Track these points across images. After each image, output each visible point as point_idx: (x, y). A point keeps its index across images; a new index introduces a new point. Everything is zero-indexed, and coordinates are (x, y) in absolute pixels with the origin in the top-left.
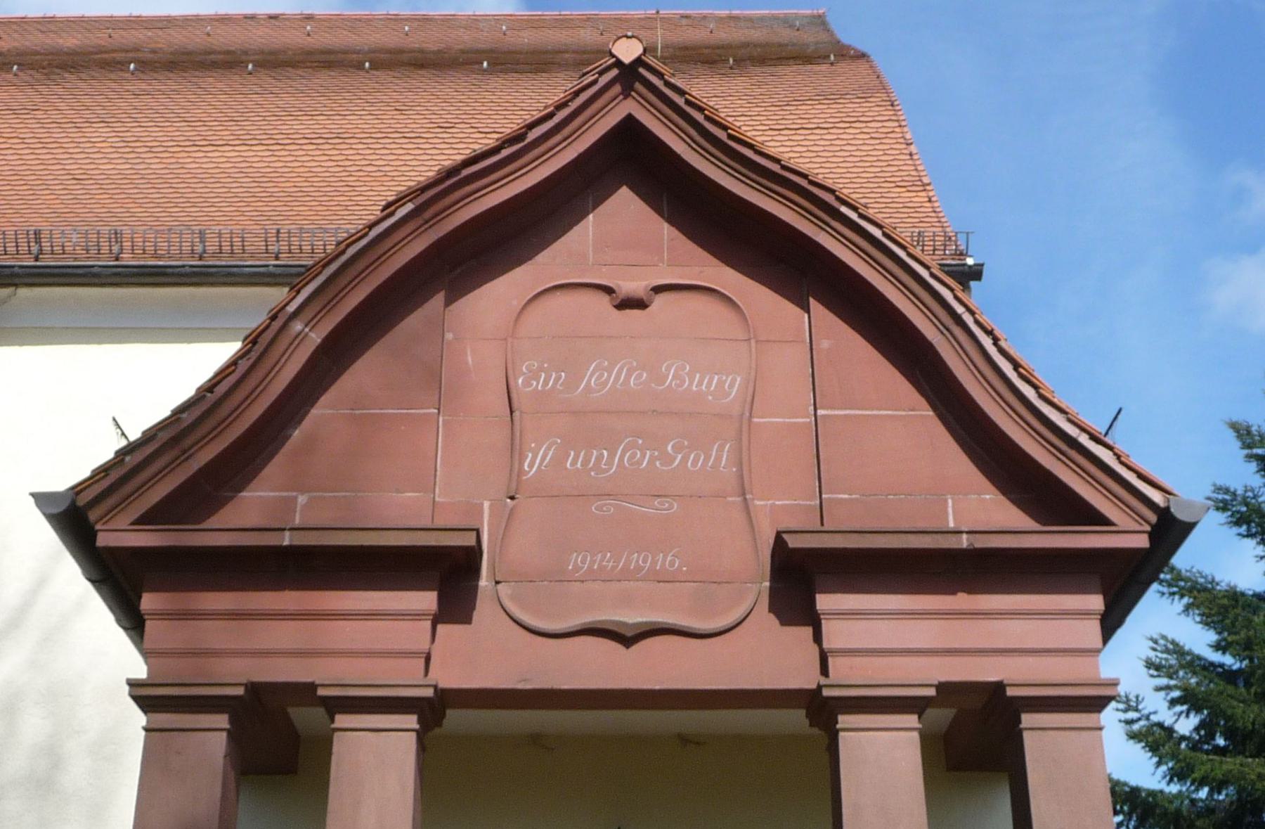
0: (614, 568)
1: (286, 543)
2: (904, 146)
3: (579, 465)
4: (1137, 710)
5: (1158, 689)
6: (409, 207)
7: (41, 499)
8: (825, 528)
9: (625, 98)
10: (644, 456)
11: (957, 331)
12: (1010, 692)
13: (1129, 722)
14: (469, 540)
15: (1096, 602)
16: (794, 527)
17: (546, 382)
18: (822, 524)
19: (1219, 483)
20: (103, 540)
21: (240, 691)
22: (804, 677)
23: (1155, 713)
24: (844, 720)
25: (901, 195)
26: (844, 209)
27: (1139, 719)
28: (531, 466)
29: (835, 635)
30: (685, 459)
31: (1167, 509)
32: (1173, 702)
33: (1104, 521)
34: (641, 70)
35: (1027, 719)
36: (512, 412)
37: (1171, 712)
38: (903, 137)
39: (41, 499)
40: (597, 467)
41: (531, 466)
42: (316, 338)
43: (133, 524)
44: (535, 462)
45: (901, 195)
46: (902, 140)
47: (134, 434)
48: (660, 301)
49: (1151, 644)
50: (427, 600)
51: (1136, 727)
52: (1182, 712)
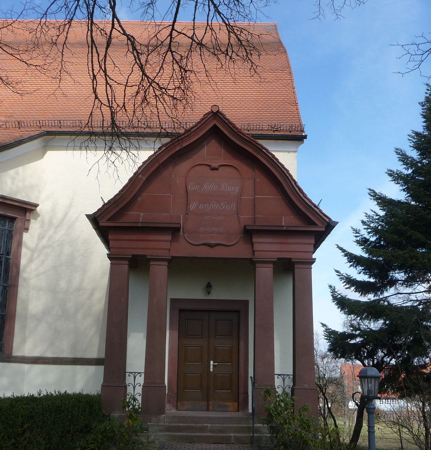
0: (209, 231)
1: (140, 226)
2: (292, 89)
3: (202, 208)
4: (359, 233)
5: (365, 229)
6: (165, 148)
7: (88, 216)
8: (256, 224)
9: (214, 120)
10: (216, 205)
11: (287, 180)
12: (293, 260)
13: (356, 237)
14: (179, 226)
15: (313, 241)
16: (248, 224)
17: (195, 188)
18: (255, 224)
19: (389, 168)
20: (101, 224)
21: (131, 257)
22: (248, 256)
23: (364, 235)
24: (257, 265)
25: (290, 107)
26: (263, 150)
27: (359, 236)
28: (191, 208)
29: (257, 247)
30: (225, 207)
31: (329, 223)
32: (369, 233)
33: (316, 225)
34: (218, 114)
35: (296, 266)
36: (187, 195)
37: (368, 236)
38: (292, 86)
39: (88, 216)
40: (206, 208)
41: (191, 208)
42: (144, 178)
43: (107, 221)
44: (193, 206)
45: (290, 107)
46: (292, 87)
47: (106, 202)
48: (221, 169)
49: (365, 215)
50: (169, 237)
51: (358, 239)
52: (371, 236)
